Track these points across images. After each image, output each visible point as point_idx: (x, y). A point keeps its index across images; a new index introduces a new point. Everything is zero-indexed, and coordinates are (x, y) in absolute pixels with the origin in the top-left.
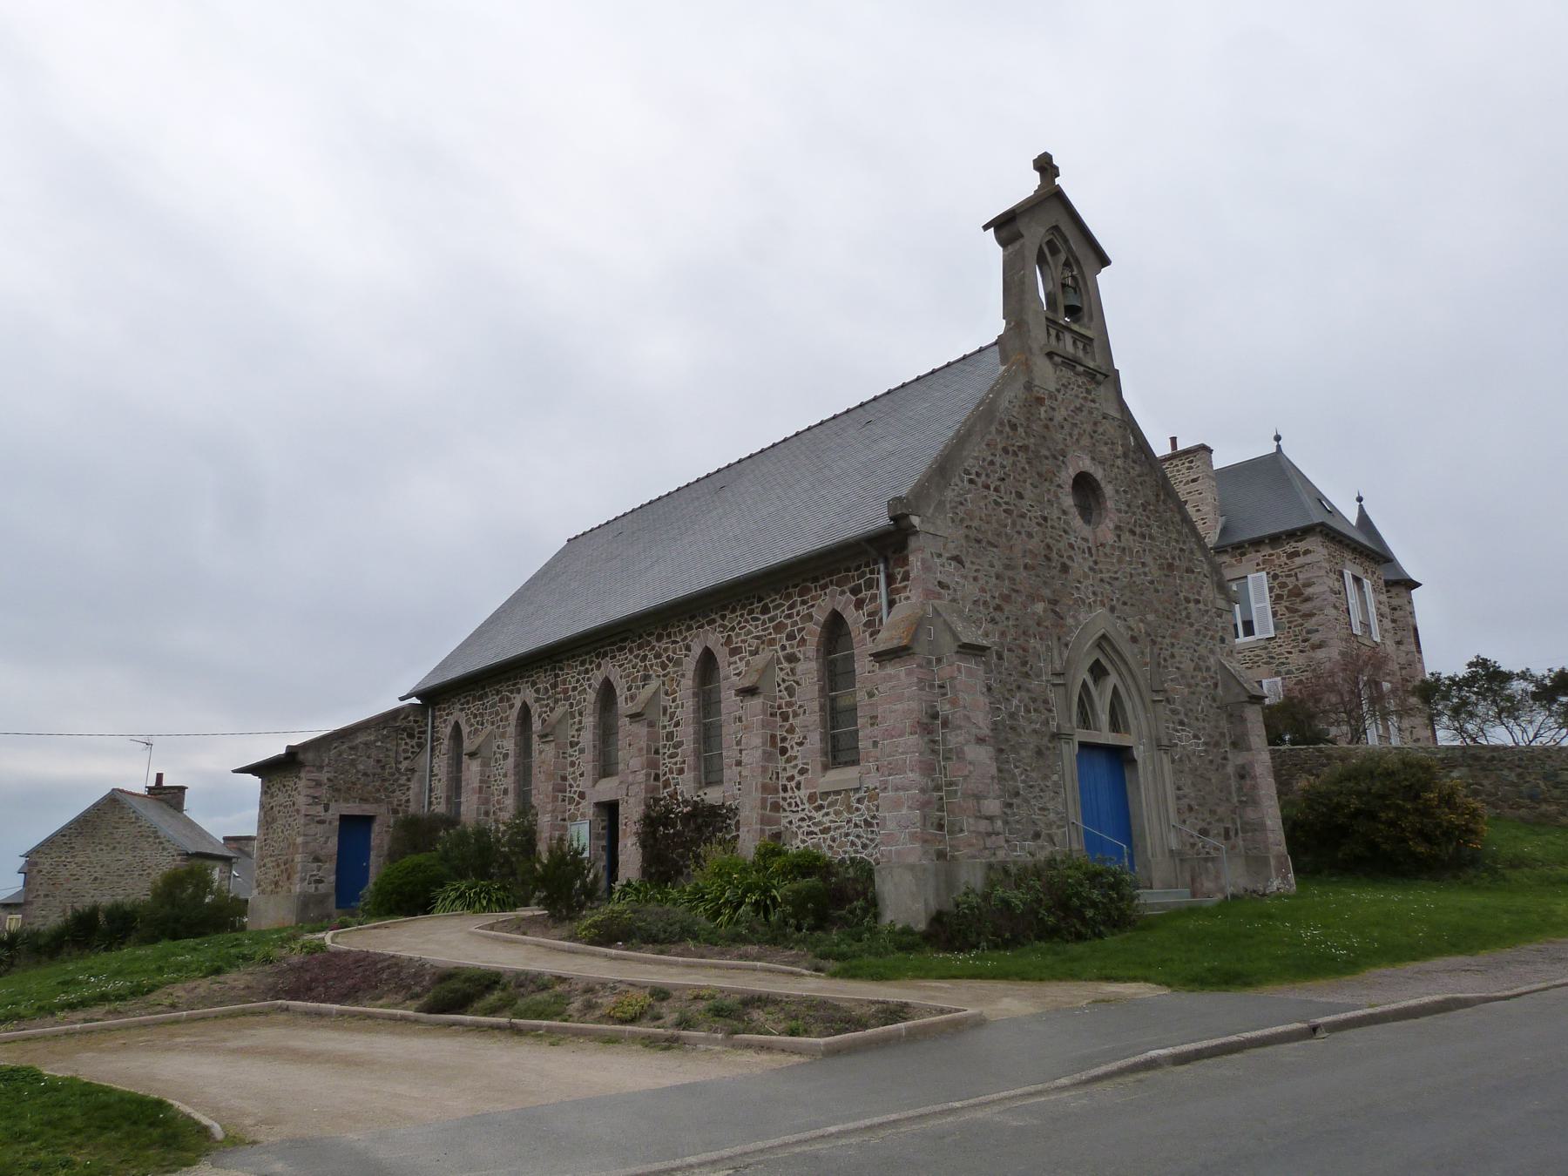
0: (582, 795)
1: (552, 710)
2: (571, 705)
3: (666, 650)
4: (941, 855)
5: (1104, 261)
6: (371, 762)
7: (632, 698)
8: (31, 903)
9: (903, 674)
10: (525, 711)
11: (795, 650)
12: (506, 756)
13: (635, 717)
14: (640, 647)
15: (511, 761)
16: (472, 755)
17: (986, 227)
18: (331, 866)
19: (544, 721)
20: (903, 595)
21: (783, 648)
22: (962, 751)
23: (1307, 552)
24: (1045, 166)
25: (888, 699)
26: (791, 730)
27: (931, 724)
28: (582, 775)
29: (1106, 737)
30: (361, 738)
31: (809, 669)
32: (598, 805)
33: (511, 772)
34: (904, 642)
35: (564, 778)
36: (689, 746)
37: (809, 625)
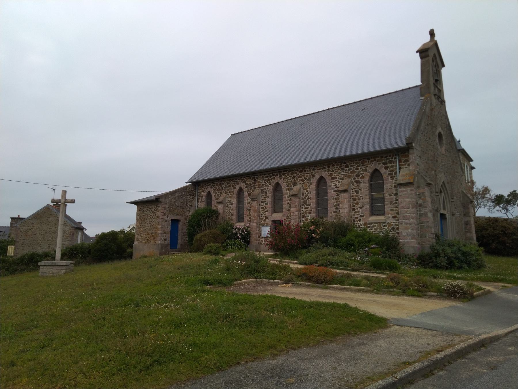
0: (267, 218)
1: (253, 191)
2: (262, 190)
3: (304, 176)
6: (179, 202)
8: (18, 242)
9: (409, 191)
11: (360, 180)
12: (232, 204)
14: (292, 174)
15: (234, 205)
18: (169, 235)
20: (404, 167)
22: (427, 214)
24: (432, 33)
28: (266, 211)
30: (177, 195)
31: (365, 186)
32: (272, 221)
33: (235, 209)
34: (411, 181)
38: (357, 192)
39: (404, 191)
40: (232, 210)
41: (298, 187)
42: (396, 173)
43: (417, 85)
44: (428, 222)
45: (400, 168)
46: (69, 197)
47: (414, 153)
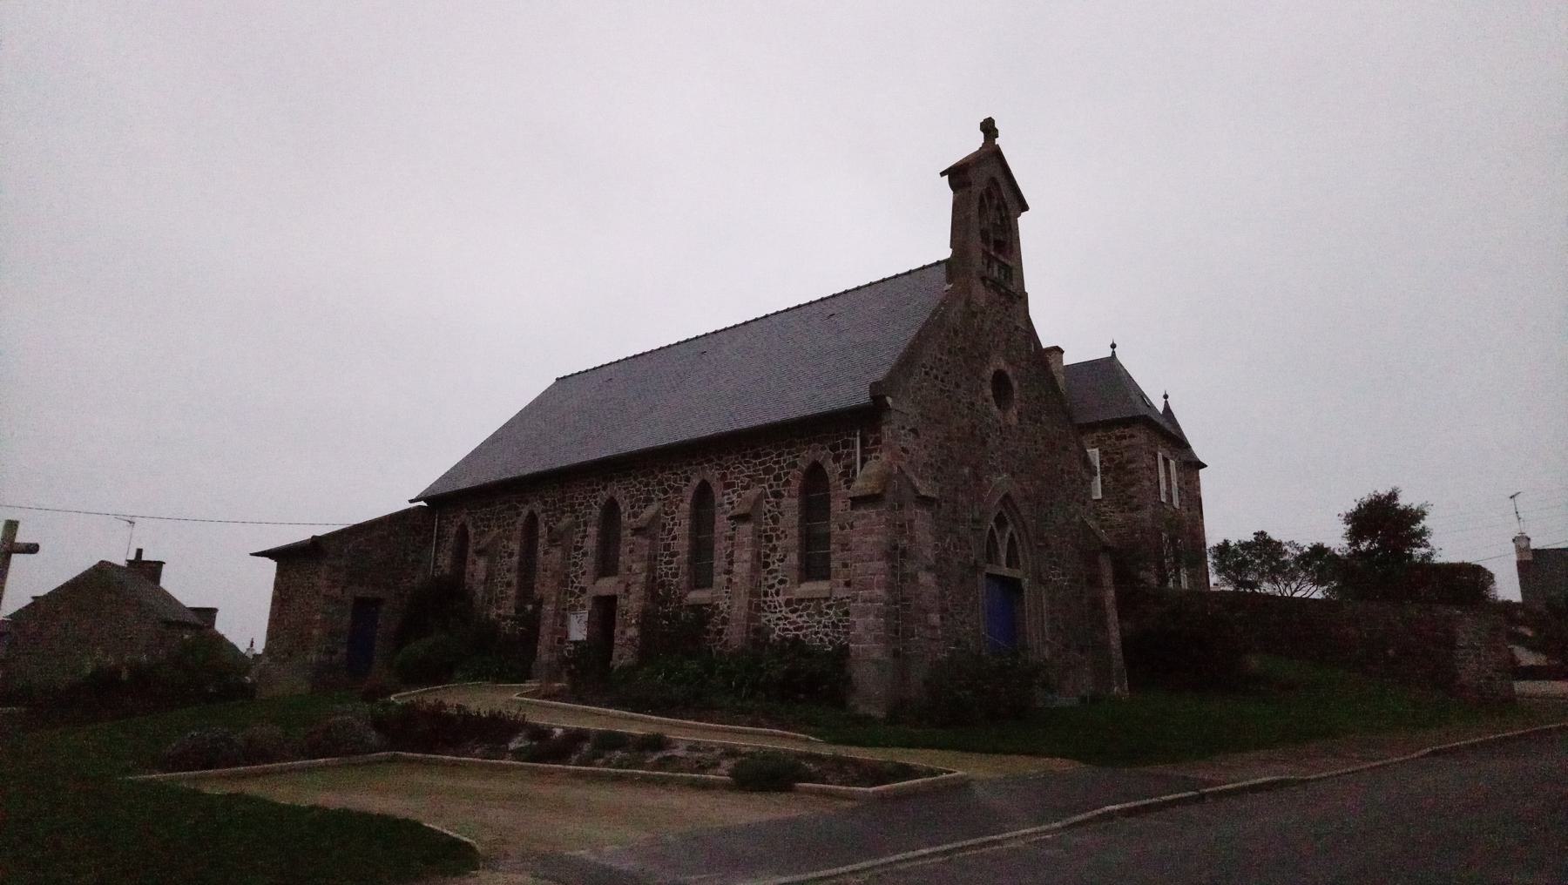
0: (583, 590)
1: (559, 520)
4: (896, 654)
5: (1025, 208)
7: (635, 515)
10: (532, 519)
12: (511, 555)
13: (637, 531)
15: (515, 559)
16: (480, 553)
17: (942, 174)
19: (550, 529)
21: (771, 486)
23: (1132, 436)
24: (989, 128)
25: (861, 537)
26: (774, 549)
27: (895, 555)
29: (1004, 571)
31: (791, 506)
35: (567, 576)
36: (683, 556)
37: (796, 472)
38: (775, 520)
39: (864, 517)
40: (675, 575)
41: (650, 511)
42: (855, 472)
43: (942, 258)
44: (918, 596)
45: (864, 461)
46: (22, 537)
47: (890, 422)
